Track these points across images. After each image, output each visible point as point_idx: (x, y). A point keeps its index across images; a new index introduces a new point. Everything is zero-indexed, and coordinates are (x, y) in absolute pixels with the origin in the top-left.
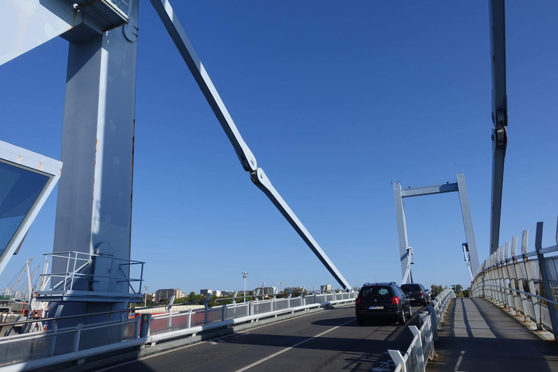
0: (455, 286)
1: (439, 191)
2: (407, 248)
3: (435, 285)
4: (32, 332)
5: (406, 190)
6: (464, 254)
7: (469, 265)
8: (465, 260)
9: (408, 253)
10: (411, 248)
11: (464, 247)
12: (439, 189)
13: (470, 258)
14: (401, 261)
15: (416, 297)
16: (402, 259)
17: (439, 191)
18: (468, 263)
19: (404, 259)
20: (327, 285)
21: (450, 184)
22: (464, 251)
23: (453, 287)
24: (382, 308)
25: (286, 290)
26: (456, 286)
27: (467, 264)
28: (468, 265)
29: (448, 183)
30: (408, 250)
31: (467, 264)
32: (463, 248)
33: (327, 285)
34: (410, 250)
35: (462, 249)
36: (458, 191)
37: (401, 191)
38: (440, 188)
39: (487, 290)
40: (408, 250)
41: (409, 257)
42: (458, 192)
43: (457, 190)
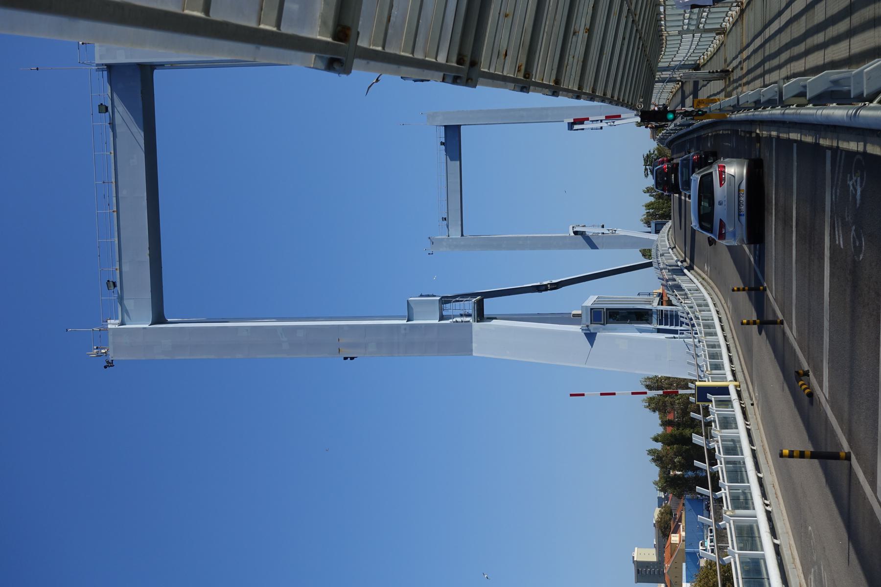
0: (646, 169)
1: (458, 162)
2: (572, 234)
3: (643, 217)
4: (669, 253)
5: (448, 227)
6: (588, 129)
7: (614, 122)
8: (601, 128)
9: (582, 234)
10: (571, 227)
11: (576, 127)
12: (453, 162)
13: (598, 121)
14: (597, 248)
15: (696, 515)
16: (593, 246)
18: (609, 124)
19: (595, 241)
20: (634, 562)
21: (446, 140)
22: (583, 129)
23: (649, 173)
24: (673, 175)
25: (654, 411)
26: (647, 167)
27: (611, 125)
28: (612, 123)
29: (442, 144)
30: (576, 233)
31: (611, 125)
32: (577, 130)
33: (634, 562)
34: (575, 230)
35: (578, 131)
36: (461, 125)
37: (449, 236)
38: (452, 159)
39: (701, 40)
40: (576, 233)
41: (589, 231)
42: (462, 126)
43: (458, 127)
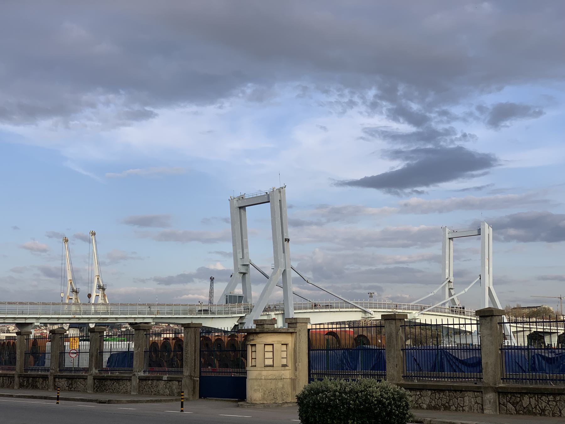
17: (454, 238)
